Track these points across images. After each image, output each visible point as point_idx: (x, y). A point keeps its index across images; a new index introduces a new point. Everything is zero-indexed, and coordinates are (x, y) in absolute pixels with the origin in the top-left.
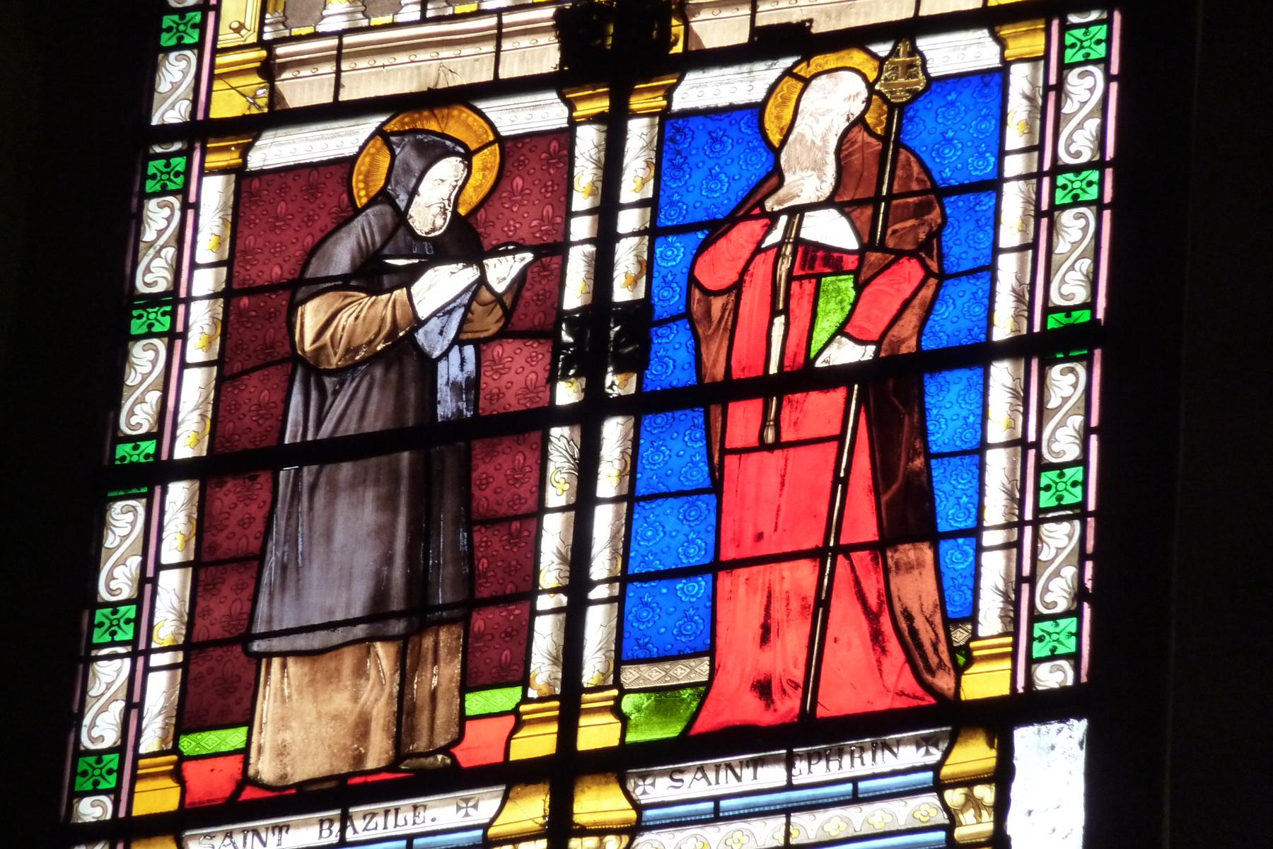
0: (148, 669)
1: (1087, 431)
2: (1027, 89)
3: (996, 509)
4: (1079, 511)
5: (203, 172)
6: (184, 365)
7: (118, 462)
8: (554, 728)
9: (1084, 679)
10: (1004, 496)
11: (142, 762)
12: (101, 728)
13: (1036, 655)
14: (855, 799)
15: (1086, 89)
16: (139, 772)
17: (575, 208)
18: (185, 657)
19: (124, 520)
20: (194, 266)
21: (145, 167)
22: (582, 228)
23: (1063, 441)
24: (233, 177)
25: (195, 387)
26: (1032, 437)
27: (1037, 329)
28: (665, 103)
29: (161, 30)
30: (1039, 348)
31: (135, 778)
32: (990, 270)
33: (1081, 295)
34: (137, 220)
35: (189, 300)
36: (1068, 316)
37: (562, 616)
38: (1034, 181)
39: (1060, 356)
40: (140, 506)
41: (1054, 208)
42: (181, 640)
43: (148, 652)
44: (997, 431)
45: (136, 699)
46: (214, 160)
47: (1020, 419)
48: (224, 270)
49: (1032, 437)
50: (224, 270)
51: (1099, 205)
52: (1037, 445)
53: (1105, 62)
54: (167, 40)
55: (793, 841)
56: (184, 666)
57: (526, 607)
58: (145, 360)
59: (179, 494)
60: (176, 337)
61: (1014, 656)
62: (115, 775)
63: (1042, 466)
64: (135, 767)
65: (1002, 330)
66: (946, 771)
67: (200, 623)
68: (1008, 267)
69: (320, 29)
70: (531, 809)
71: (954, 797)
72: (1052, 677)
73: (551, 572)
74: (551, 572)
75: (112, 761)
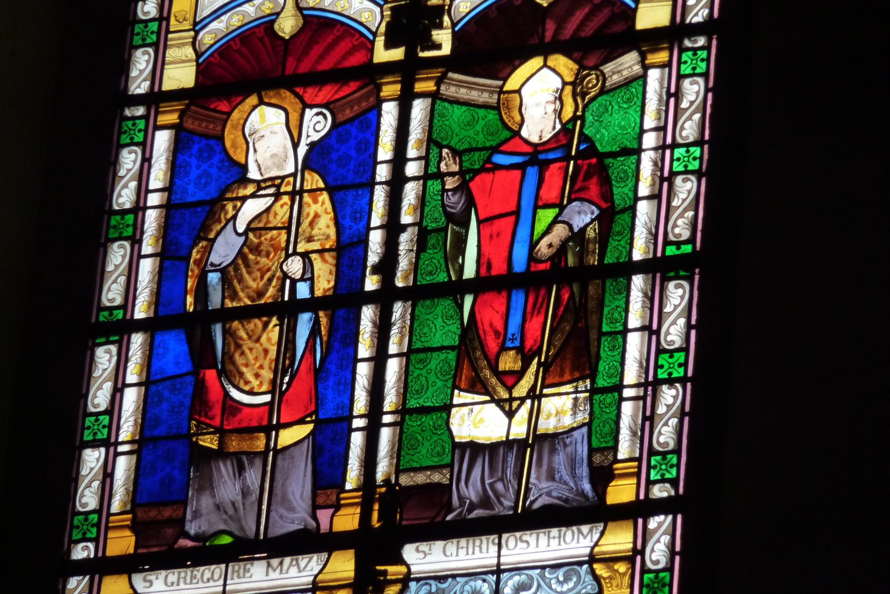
0: (117, 454)
1: (689, 326)
2: (637, 355)
3: (631, 375)
4: (683, 380)
6: (140, 257)
8: (358, 510)
9: (716, 14)
10: (651, 164)
11: (111, 518)
12: (88, 498)
13: (683, 354)
15: (693, 91)
16: (110, 525)
17: (372, 225)
18: (139, 447)
19: (105, 358)
20: (148, 191)
21: (133, 30)
22: (383, 172)
23: (674, 332)
24: (158, 259)
25: (147, 268)
26: (655, 327)
27: (659, 254)
28: (435, 88)
30: (660, 268)
31: (107, 529)
32: (633, 209)
33: (686, 235)
34: (114, 163)
35: (145, 208)
36: (678, 248)
37: (372, 364)
38: (660, 151)
39: (672, 274)
40: (114, 349)
41: (673, 174)
42: (129, 508)
43: (117, 443)
44: (634, 321)
45: (109, 470)
47: (652, 247)
48: (166, 194)
49: (655, 327)
50: (134, 457)
51: (698, 173)
52: (658, 332)
53: (705, 75)
54: (137, 40)
55: (335, 529)
57: (345, 425)
58: (117, 255)
59: (137, 340)
60: (136, 241)
61: (638, 475)
62: (142, 133)
63: (660, 351)
64: (107, 522)
65: (637, 256)
67: (156, 364)
68: (644, 209)
70: (343, 565)
72: (659, 492)
73: (361, 403)
75: (94, 518)
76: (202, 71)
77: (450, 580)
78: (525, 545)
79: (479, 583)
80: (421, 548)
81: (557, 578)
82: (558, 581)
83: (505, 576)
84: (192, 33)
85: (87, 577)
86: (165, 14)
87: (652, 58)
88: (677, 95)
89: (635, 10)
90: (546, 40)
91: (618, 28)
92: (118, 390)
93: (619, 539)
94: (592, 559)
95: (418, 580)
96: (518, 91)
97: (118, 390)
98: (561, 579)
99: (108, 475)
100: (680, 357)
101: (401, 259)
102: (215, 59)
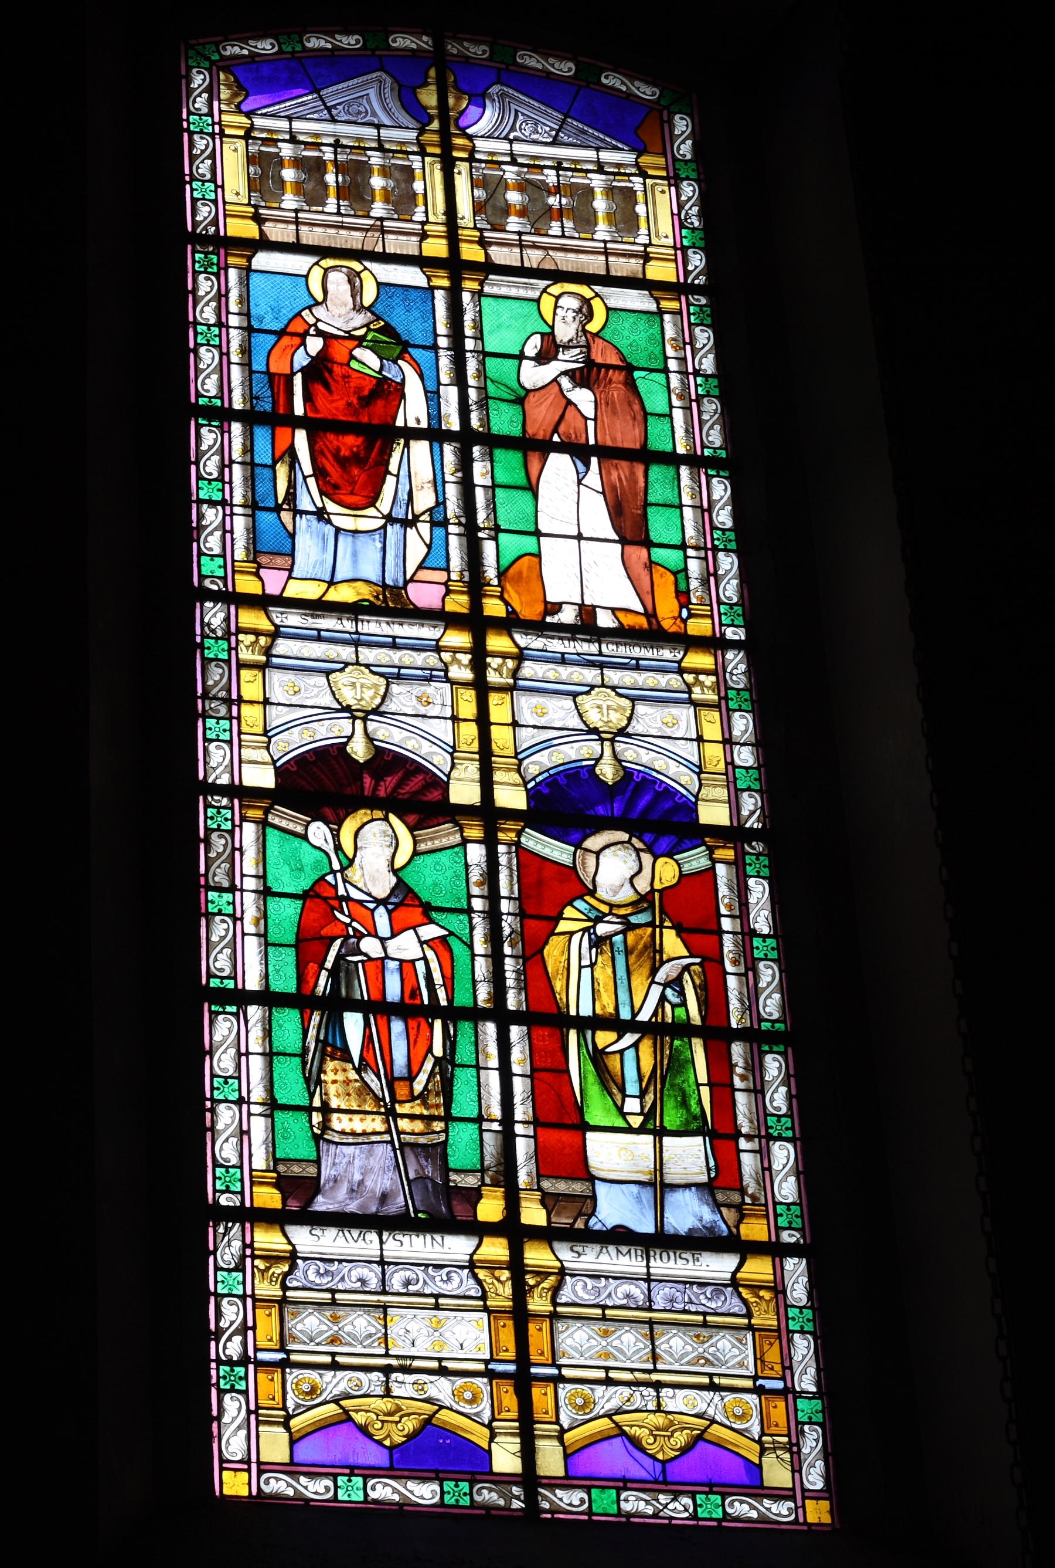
14: (637, 668)
26: (759, 1088)
69: (637, 241)
71: (446, 656)
77: (603, 1279)
78: (685, 1262)
79: (632, 1287)
80: (397, 1237)
81: (705, 1293)
82: (318, 1272)
83: (378, 1269)
84: (265, 739)
89: (447, 784)
90: (366, 793)
91: (435, 795)
93: (759, 1269)
94: (472, 1265)
95: (305, 1259)
96: (598, 854)
98: (445, 1278)
102: (638, 777)
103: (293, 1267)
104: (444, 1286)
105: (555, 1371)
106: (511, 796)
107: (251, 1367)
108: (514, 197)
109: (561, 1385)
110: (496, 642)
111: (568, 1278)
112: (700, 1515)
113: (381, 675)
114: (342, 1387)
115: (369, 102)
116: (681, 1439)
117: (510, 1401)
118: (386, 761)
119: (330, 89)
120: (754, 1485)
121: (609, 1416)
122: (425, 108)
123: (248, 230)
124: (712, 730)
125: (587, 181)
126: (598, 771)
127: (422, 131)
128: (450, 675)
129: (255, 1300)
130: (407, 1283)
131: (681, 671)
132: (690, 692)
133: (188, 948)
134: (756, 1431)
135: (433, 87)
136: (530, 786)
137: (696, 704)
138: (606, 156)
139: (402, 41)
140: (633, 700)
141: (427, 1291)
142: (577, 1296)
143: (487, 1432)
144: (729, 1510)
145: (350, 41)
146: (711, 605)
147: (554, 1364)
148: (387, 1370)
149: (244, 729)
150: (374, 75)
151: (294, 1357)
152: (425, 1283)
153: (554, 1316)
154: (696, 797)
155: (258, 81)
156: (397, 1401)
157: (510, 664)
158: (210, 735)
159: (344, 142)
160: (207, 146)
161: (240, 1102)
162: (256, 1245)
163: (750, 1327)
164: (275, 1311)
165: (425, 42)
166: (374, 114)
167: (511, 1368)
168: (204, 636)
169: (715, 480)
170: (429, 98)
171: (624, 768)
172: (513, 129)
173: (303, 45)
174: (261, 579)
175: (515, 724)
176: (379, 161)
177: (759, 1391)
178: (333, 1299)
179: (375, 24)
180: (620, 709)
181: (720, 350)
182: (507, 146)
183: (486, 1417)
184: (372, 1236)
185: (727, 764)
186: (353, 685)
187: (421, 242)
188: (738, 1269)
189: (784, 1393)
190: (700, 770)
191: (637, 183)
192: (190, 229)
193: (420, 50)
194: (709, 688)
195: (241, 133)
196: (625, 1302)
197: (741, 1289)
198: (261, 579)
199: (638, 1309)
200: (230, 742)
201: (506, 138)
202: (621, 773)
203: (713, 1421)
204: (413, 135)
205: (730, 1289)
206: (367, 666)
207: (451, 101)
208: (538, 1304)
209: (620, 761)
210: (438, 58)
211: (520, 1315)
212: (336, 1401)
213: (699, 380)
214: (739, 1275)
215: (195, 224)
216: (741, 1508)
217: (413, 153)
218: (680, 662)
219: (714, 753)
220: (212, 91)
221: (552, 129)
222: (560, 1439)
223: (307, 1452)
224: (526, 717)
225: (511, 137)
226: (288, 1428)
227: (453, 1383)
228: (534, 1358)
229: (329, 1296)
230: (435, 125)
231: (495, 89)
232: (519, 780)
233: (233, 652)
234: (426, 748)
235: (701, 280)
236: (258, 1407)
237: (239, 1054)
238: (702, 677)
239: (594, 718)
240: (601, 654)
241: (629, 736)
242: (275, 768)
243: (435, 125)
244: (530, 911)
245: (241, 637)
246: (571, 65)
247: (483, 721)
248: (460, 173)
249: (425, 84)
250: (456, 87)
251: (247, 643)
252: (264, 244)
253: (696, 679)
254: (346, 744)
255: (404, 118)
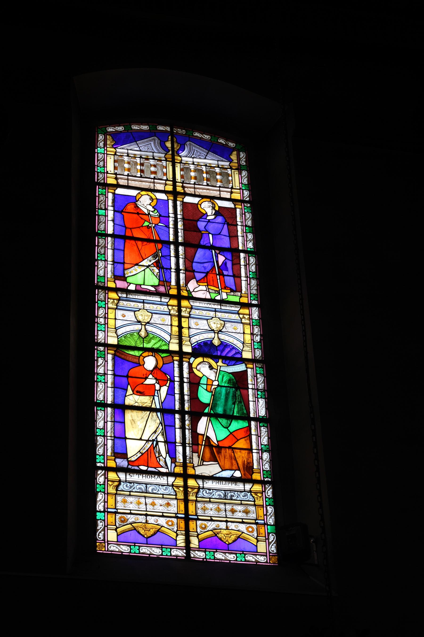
5: (108, 353)
7: (96, 347)
13: (170, 555)
19: (100, 414)
29: (96, 459)
46: (110, 191)
55: (175, 472)
56: (115, 354)
60: (106, 383)
66: (168, 303)
73: (173, 266)
74: (173, 266)
76: (193, 348)
77: (212, 490)
79: (220, 493)
85: (104, 471)
86: (106, 323)
87: (248, 366)
88: (261, 458)
89: (242, 352)
91: (238, 356)
92: (105, 422)
97: (105, 422)
99: (105, 445)
100: (169, 554)
101: (186, 404)
103: (120, 484)
104: (164, 491)
105: (196, 517)
106: (187, 349)
107: (106, 513)
108: (193, 174)
109: (117, 515)
110: (184, 303)
111: (122, 483)
112: (238, 560)
113: (223, 321)
114: (214, 526)
115: (151, 145)
116: (233, 537)
117: (182, 524)
118: (224, 345)
119: (140, 141)
120: (256, 553)
121: (131, 524)
122: (167, 148)
123: (114, 182)
124: (248, 330)
125: (135, 160)
126: (213, 342)
127: (166, 154)
128: (171, 313)
129: (108, 494)
130: (152, 490)
131: (239, 314)
132: (241, 320)
133: (92, 391)
134: (256, 535)
135: (170, 142)
136: (193, 345)
137: (244, 324)
138: (221, 163)
139: (161, 128)
140: (152, 313)
141: (238, 499)
142: (124, 488)
143: (175, 534)
144: (246, 559)
145: (145, 128)
146: (248, 294)
147: (115, 508)
148: (146, 515)
149: (109, 326)
150: (152, 138)
151: (119, 511)
152: (158, 490)
153: (196, 501)
154: (242, 350)
155: (119, 140)
156: (230, 531)
157: (188, 310)
158: (99, 329)
159: (143, 157)
160: (102, 157)
161: (104, 436)
162: (109, 478)
163: (176, 499)
164: (114, 497)
165: (168, 129)
166: (152, 149)
167: (183, 516)
168: (98, 300)
169: (100, 240)
170: (168, 144)
171: (221, 341)
172: (193, 154)
173: (218, 141)
174: (116, 283)
175: (189, 328)
176: (219, 171)
177: (257, 524)
178: (210, 500)
179: (152, 121)
180: (221, 324)
181: (253, 220)
182: (126, 151)
183: (175, 529)
184: (165, 478)
185: (251, 340)
186: (142, 315)
187: (231, 194)
188: (251, 488)
189: (264, 524)
190: (171, 335)
191: (229, 171)
192: (96, 181)
193: (166, 131)
194: (247, 319)
195: (113, 153)
196: (218, 497)
197: (174, 487)
198: (116, 283)
199: (142, 492)
200: (105, 331)
201: (191, 157)
202: (220, 343)
203: (243, 533)
204: (163, 155)
205: (171, 487)
206: (146, 310)
207: (175, 146)
208: (192, 497)
209: (220, 339)
210: (171, 133)
211: (186, 501)
212: (212, 531)
213: (247, 228)
214: (252, 489)
215: (98, 180)
216: (250, 558)
217: (164, 160)
218: (238, 311)
219: (248, 338)
220: (105, 141)
221: (205, 155)
222: (197, 537)
223: (121, 538)
224: (193, 325)
225: (193, 156)
226: (117, 531)
227: (166, 519)
228: (190, 513)
229: (240, 502)
230: (170, 153)
231: (188, 143)
232: (116, 336)
233: (107, 305)
234: (235, 342)
235: (248, 199)
236: (108, 525)
237: (105, 422)
238: (245, 316)
239: (140, 318)
240: (221, 309)
241: (222, 332)
242: (192, 347)
243: (170, 153)
244: (117, 374)
245: (109, 300)
246: (147, 126)
247: (180, 327)
248: (177, 167)
249: (168, 141)
250: (177, 142)
251: (111, 302)
252: (118, 186)
253: (243, 316)
254: (212, 340)
255: (163, 151)
